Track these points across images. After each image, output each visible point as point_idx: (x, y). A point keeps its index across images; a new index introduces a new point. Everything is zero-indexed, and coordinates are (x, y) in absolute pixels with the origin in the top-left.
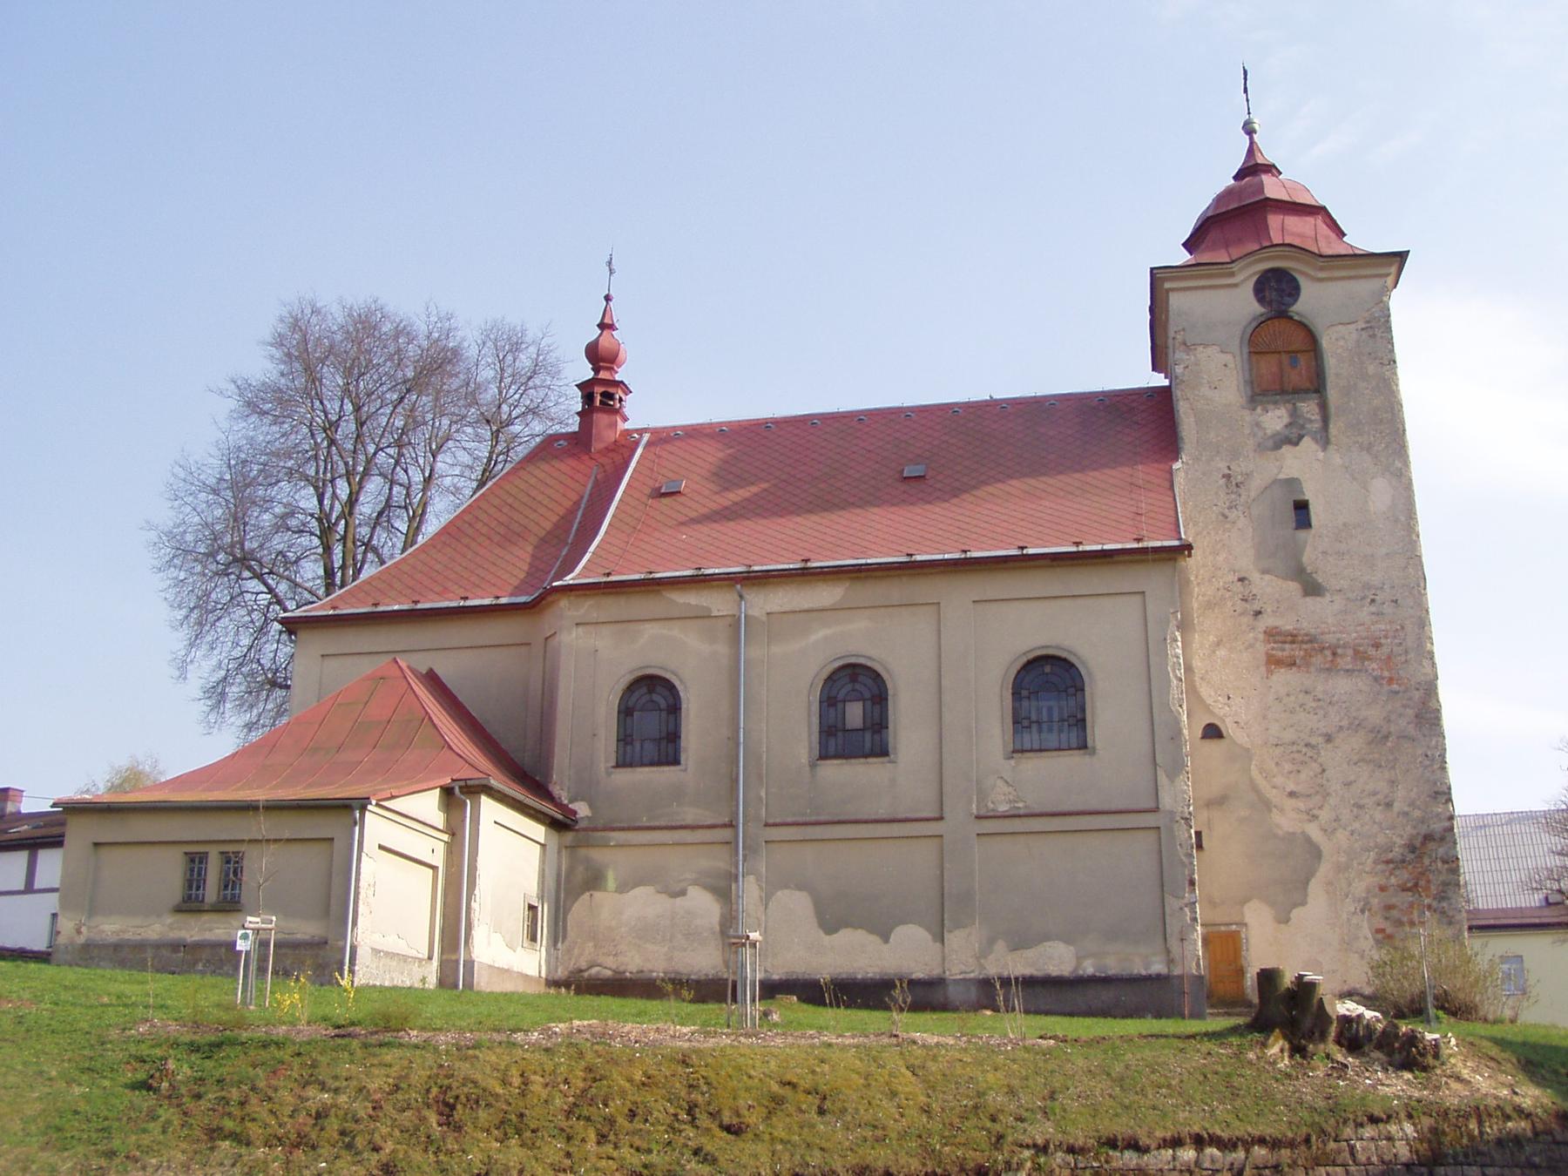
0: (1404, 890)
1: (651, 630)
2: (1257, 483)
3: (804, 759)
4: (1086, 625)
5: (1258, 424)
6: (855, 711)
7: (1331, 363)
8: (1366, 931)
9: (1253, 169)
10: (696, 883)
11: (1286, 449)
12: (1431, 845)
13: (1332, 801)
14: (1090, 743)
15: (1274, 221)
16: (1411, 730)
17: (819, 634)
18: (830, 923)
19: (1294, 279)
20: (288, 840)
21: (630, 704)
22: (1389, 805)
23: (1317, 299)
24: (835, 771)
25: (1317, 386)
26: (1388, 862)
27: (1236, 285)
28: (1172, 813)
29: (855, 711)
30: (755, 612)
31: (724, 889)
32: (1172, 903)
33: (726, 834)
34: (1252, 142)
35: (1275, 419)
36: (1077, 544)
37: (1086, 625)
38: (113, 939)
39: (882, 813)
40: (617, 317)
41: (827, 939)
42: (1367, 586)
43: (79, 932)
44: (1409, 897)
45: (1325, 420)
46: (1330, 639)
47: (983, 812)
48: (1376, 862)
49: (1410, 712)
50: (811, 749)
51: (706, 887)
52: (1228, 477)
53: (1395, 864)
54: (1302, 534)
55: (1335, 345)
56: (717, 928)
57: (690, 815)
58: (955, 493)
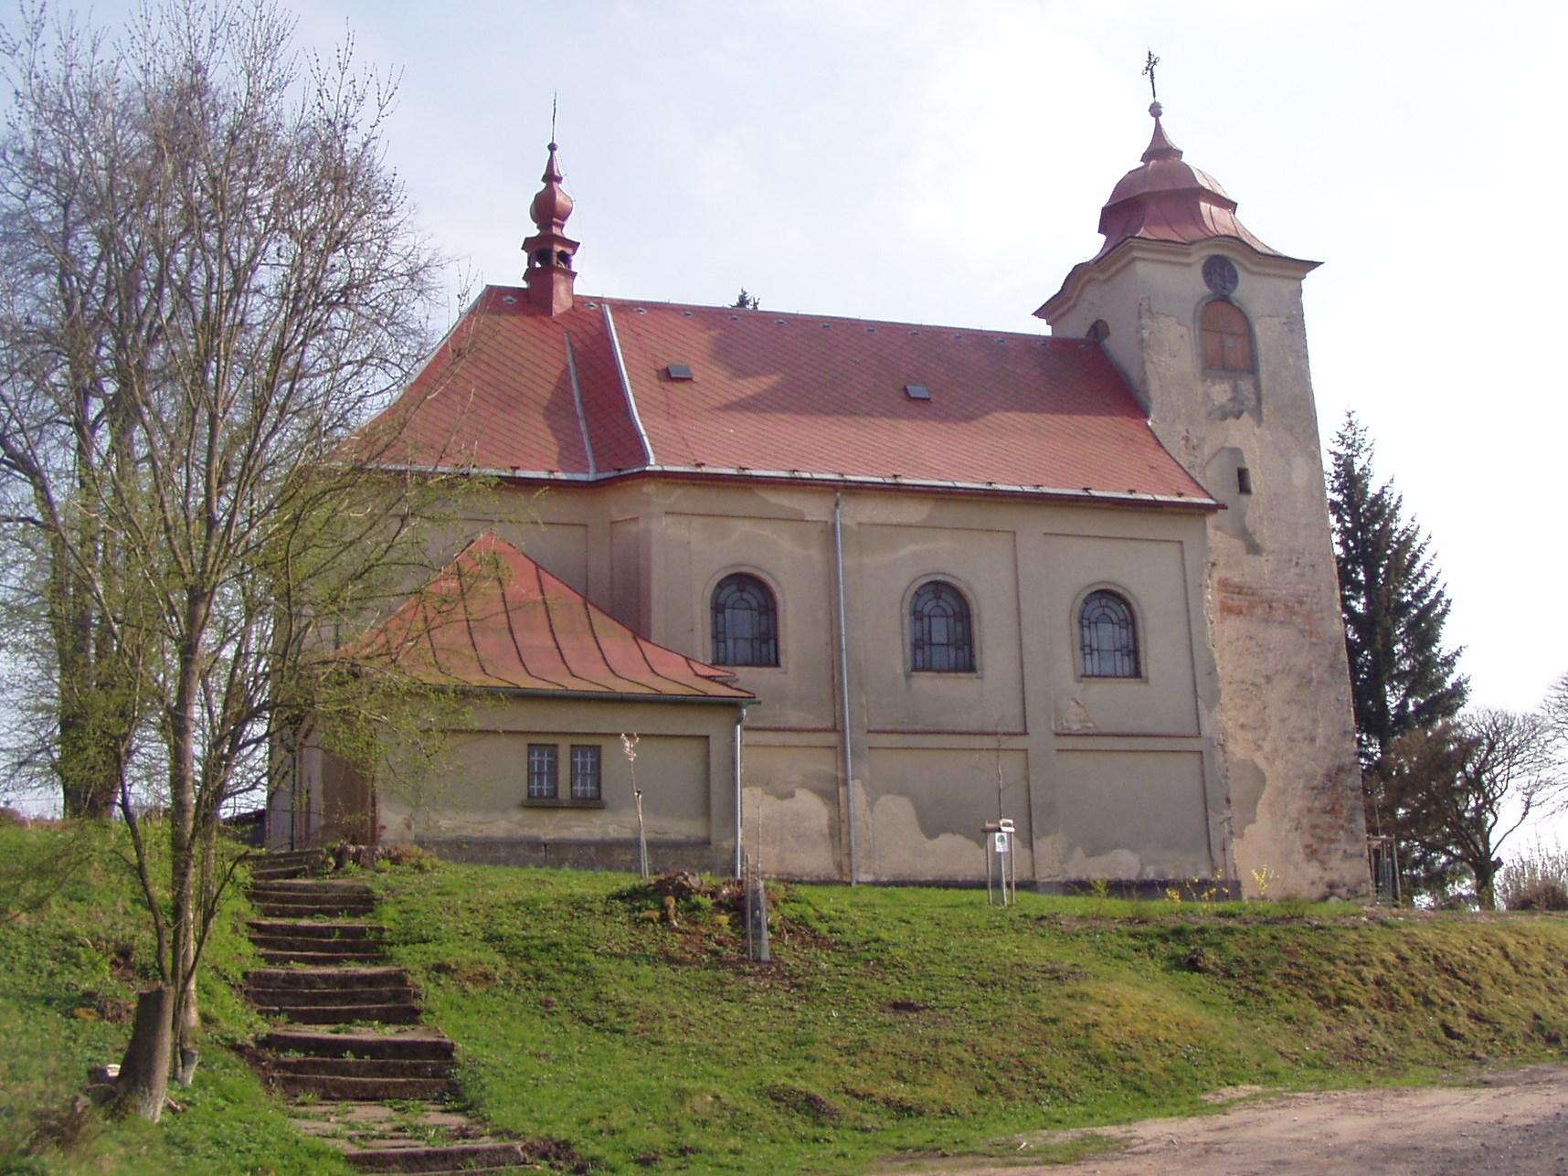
0: (1326, 812)
1: (743, 527)
2: (1207, 450)
3: (900, 669)
4: (1141, 567)
5: (1207, 395)
6: (944, 627)
7: (1262, 349)
8: (1299, 846)
9: (1160, 150)
10: (802, 786)
11: (1231, 421)
12: (1342, 775)
13: (1272, 734)
14: (977, 663)
15: (1205, 207)
16: (1327, 677)
17: (906, 551)
18: (931, 830)
19: (1232, 269)
20: (480, 732)
21: (721, 599)
22: (1313, 740)
23: (1249, 289)
24: (925, 681)
25: (1250, 366)
26: (1313, 788)
27: (1189, 265)
28: (1211, 739)
29: (944, 627)
30: (848, 522)
31: (832, 792)
32: (1214, 819)
33: (832, 738)
34: (1158, 126)
35: (1220, 393)
36: (1131, 491)
37: (1141, 567)
38: (450, 835)
39: (973, 726)
40: (560, 169)
41: (929, 844)
42: (1292, 551)
43: (409, 827)
44: (1327, 818)
45: (1259, 400)
46: (1266, 593)
47: (1059, 730)
48: (1305, 788)
49: (1326, 662)
50: (905, 661)
51: (816, 791)
52: (1187, 439)
53: (1321, 790)
54: (1244, 498)
55: (1266, 332)
56: (826, 831)
57: (794, 717)
58: (968, 418)
